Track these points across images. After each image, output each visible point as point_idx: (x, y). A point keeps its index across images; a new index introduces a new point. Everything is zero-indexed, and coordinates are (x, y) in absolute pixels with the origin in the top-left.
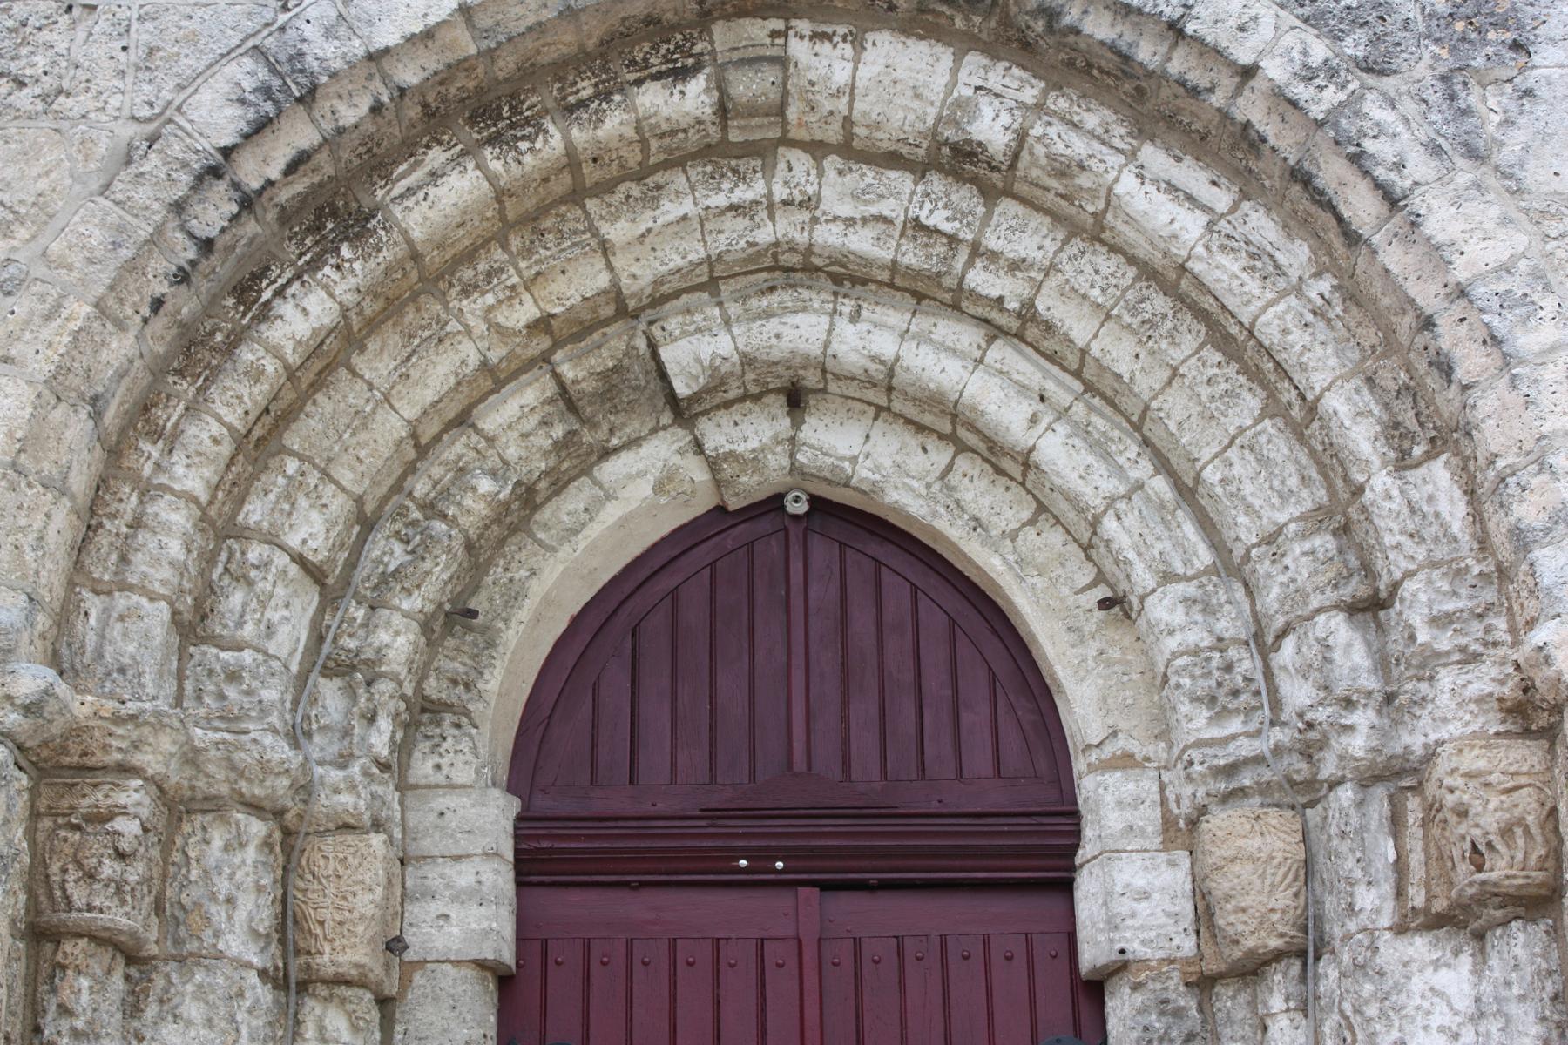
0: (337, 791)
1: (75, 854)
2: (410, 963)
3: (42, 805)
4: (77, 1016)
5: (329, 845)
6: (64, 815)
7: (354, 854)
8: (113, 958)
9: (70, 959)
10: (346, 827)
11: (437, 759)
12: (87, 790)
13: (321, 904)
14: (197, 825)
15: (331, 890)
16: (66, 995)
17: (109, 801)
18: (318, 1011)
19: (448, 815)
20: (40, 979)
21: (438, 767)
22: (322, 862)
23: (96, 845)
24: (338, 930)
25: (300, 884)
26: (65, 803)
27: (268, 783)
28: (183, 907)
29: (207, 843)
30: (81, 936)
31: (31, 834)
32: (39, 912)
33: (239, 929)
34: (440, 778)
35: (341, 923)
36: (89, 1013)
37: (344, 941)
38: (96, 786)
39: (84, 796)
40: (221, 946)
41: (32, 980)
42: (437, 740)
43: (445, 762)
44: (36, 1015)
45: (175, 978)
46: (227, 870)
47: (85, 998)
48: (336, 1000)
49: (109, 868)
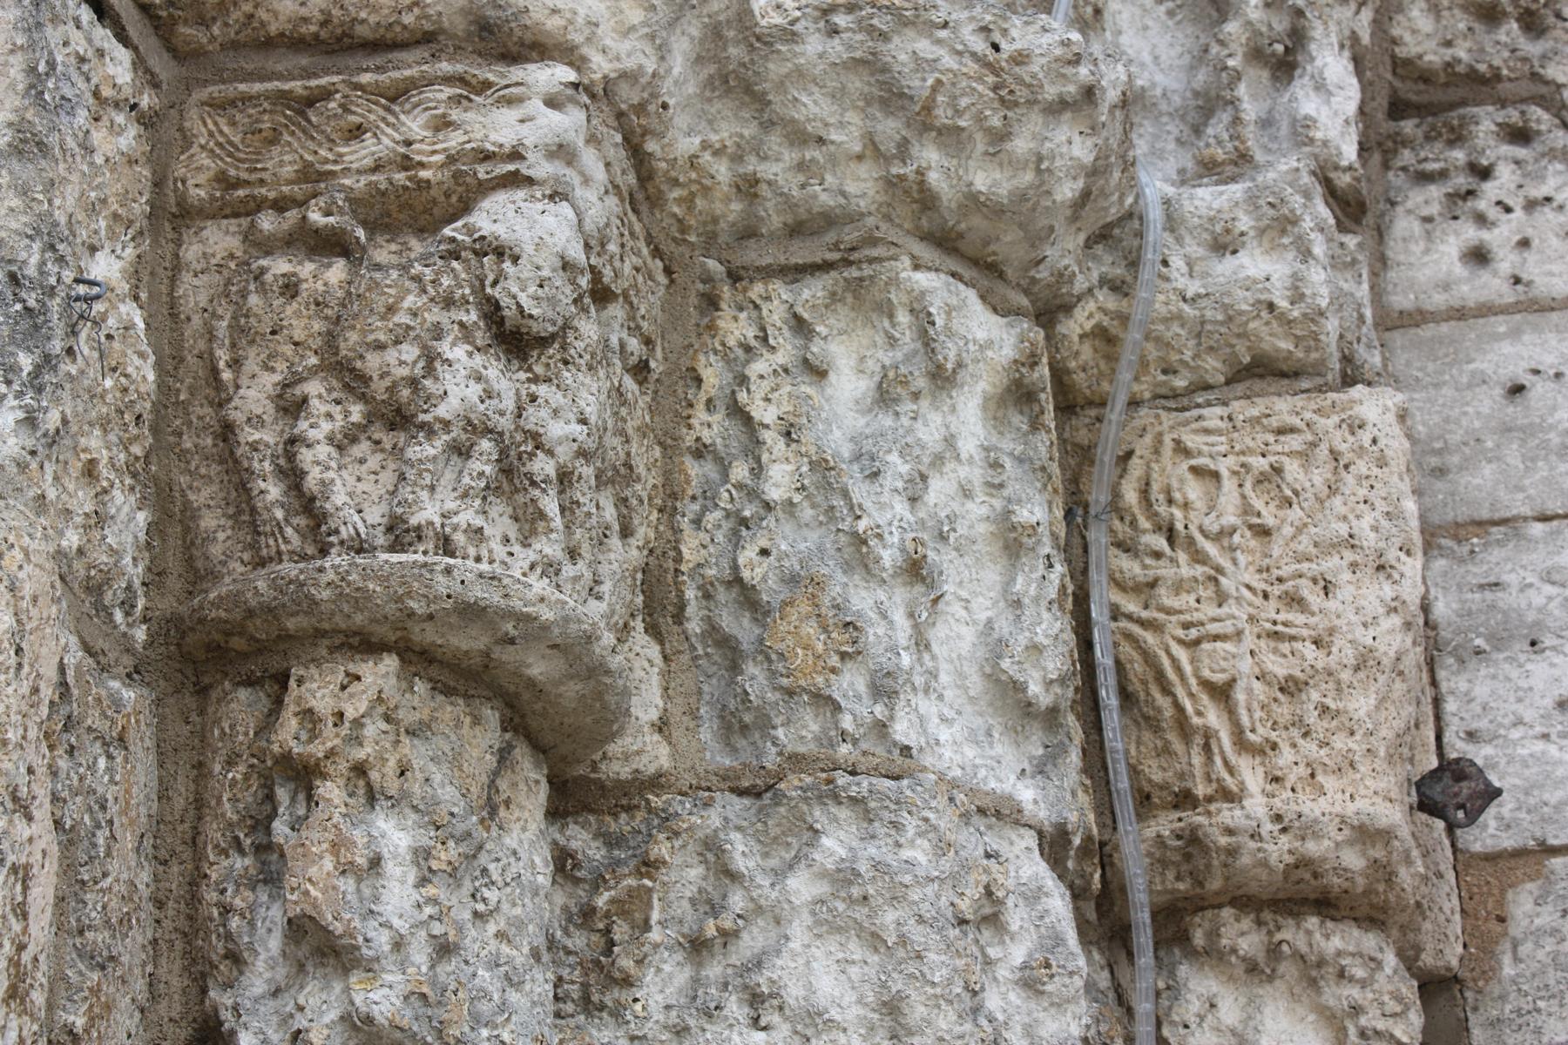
0: (1224, 244)
1: (331, 339)
2: (1492, 858)
3: (197, 177)
4: (370, 968)
5: (1213, 430)
6: (280, 206)
7: (1305, 456)
8: (504, 755)
9: (331, 738)
10: (1261, 371)
11: (1470, 233)
12: (365, 111)
13: (1219, 631)
14: (775, 314)
15: (1240, 575)
16: (316, 879)
17: (454, 140)
18: (1230, 1012)
19: (1539, 390)
20: (214, 832)
21: (1479, 256)
22: (1194, 491)
23: (406, 288)
24: (1283, 711)
25: (1131, 567)
26: (282, 164)
27: (1021, 145)
28: (748, 597)
29: (818, 373)
30: (367, 645)
31: (157, 281)
32: (198, 575)
33: (952, 668)
34: (1492, 285)
35: (1291, 688)
36: (420, 955)
37: (1310, 748)
38: (396, 95)
39: (356, 133)
40: (902, 730)
41: (180, 842)
42: (1461, 181)
43: (1500, 237)
44: (200, 977)
45: (742, 853)
46: (897, 466)
47: (398, 894)
48: (1288, 969)
49: (467, 380)
